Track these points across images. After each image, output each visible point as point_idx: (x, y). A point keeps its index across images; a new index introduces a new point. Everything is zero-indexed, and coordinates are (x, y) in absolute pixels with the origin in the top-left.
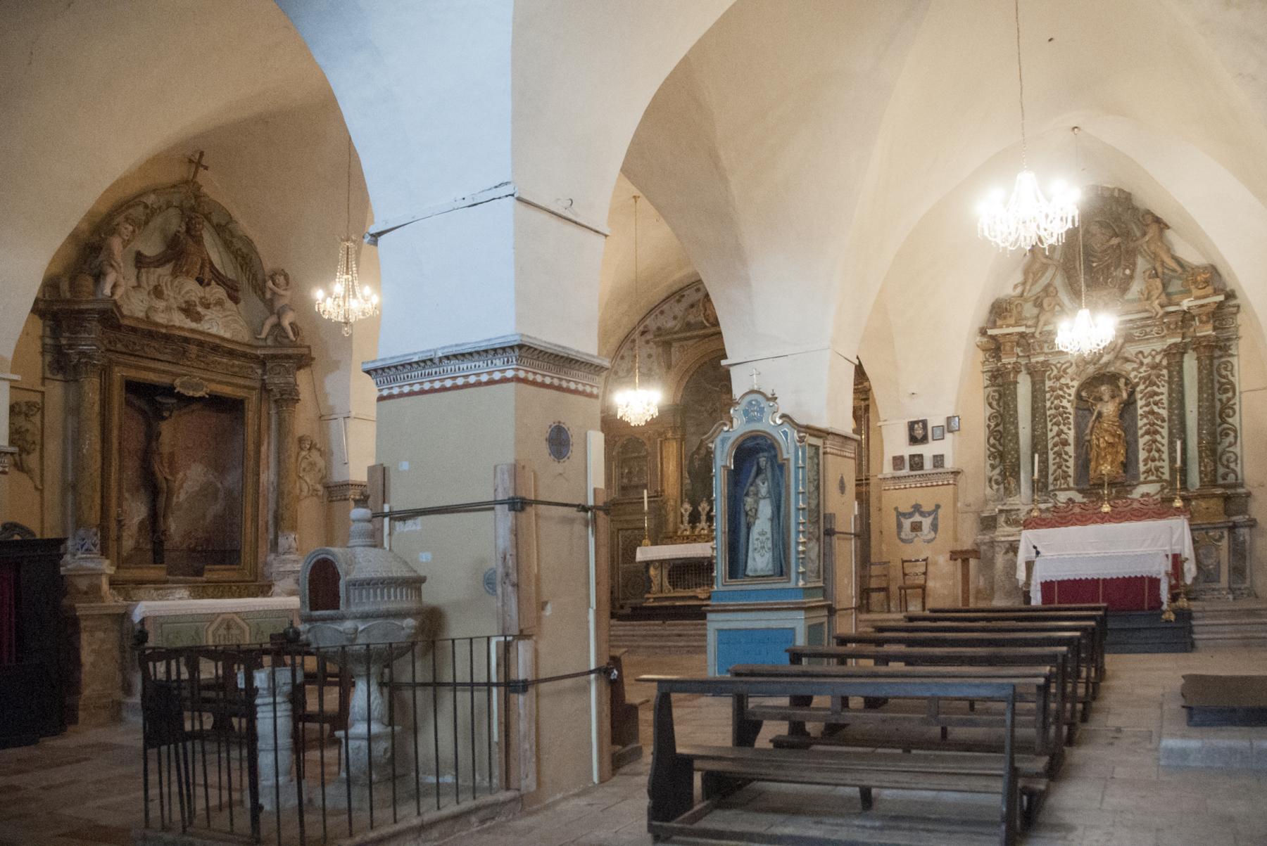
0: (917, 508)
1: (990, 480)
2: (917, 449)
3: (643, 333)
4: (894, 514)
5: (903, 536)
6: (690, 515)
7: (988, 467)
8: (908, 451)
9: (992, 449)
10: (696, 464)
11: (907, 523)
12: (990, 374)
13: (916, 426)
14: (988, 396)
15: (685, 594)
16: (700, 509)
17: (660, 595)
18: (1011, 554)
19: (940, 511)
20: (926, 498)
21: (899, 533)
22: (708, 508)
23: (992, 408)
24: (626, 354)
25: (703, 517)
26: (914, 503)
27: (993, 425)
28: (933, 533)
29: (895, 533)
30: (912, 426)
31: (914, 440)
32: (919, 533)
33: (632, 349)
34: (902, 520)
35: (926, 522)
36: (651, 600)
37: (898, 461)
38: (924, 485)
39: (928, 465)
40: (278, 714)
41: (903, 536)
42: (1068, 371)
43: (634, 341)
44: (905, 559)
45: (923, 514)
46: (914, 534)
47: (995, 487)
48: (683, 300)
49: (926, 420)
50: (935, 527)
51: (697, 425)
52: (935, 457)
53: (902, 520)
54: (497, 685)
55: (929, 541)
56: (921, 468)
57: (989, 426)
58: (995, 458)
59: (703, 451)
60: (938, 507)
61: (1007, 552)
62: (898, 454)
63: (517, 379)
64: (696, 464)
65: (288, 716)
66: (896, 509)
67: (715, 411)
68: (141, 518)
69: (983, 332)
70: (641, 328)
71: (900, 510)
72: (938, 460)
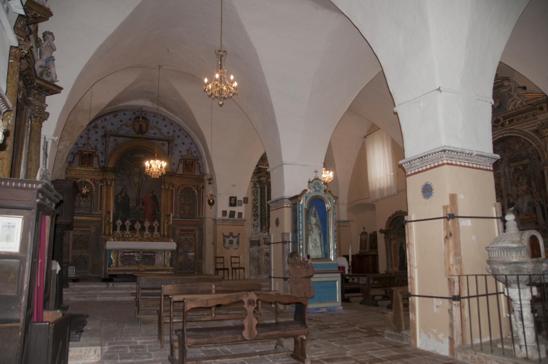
0: (231, 234)
1: (254, 225)
2: (233, 209)
3: (94, 127)
4: (222, 235)
5: (226, 246)
6: (121, 226)
7: (253, 220)
8: (229, 209)
9: (254, 213)
10: (119, 200)
11: (227, 240)
12: (254, 182)
13: (232, 199)
14: (253, 191)
15: (130, 269)
16: (126, 224)
17: (116, 269)
19: (240, 236)
20: (235, 230)
21: (224, 245)
22: (158, 225)
23: (255, 196)
25: (156, 229)
26: (230, 232)
27: (255, 203)
28: (237, 245)
29: (222, 244)
30: (231, 198)
31: (231, 205)
32: (232, 245)
33: (87, 134)
34: (226, 239)
35: (235, 240)
37: (224, 213)
38: (234, 224)
39: (236, 216)
40: (519, 302)
41: (226, 246)
42: (511, 202)
44: (232, 256)
45: (234, 237)
46: (230, 245)
47: (255, 228)
48: (117, 116)
49: (236, 197)
50: (238, 243)
52: (239, 213)
53: (226, 239)
54: (501, 293)
55: (236, 249)
56: (233, 217)
57: (253, 203)
58: (255, 216)
59: (123, 194)
60: (239, 234)
61: (265, 256)
62: (224, 209)
63: (448, 164)
64: (119, 200)
65: (528, 304)
66: (223, 233)
69: (257, 166)
71: (224, 234)
72: (240, 214)
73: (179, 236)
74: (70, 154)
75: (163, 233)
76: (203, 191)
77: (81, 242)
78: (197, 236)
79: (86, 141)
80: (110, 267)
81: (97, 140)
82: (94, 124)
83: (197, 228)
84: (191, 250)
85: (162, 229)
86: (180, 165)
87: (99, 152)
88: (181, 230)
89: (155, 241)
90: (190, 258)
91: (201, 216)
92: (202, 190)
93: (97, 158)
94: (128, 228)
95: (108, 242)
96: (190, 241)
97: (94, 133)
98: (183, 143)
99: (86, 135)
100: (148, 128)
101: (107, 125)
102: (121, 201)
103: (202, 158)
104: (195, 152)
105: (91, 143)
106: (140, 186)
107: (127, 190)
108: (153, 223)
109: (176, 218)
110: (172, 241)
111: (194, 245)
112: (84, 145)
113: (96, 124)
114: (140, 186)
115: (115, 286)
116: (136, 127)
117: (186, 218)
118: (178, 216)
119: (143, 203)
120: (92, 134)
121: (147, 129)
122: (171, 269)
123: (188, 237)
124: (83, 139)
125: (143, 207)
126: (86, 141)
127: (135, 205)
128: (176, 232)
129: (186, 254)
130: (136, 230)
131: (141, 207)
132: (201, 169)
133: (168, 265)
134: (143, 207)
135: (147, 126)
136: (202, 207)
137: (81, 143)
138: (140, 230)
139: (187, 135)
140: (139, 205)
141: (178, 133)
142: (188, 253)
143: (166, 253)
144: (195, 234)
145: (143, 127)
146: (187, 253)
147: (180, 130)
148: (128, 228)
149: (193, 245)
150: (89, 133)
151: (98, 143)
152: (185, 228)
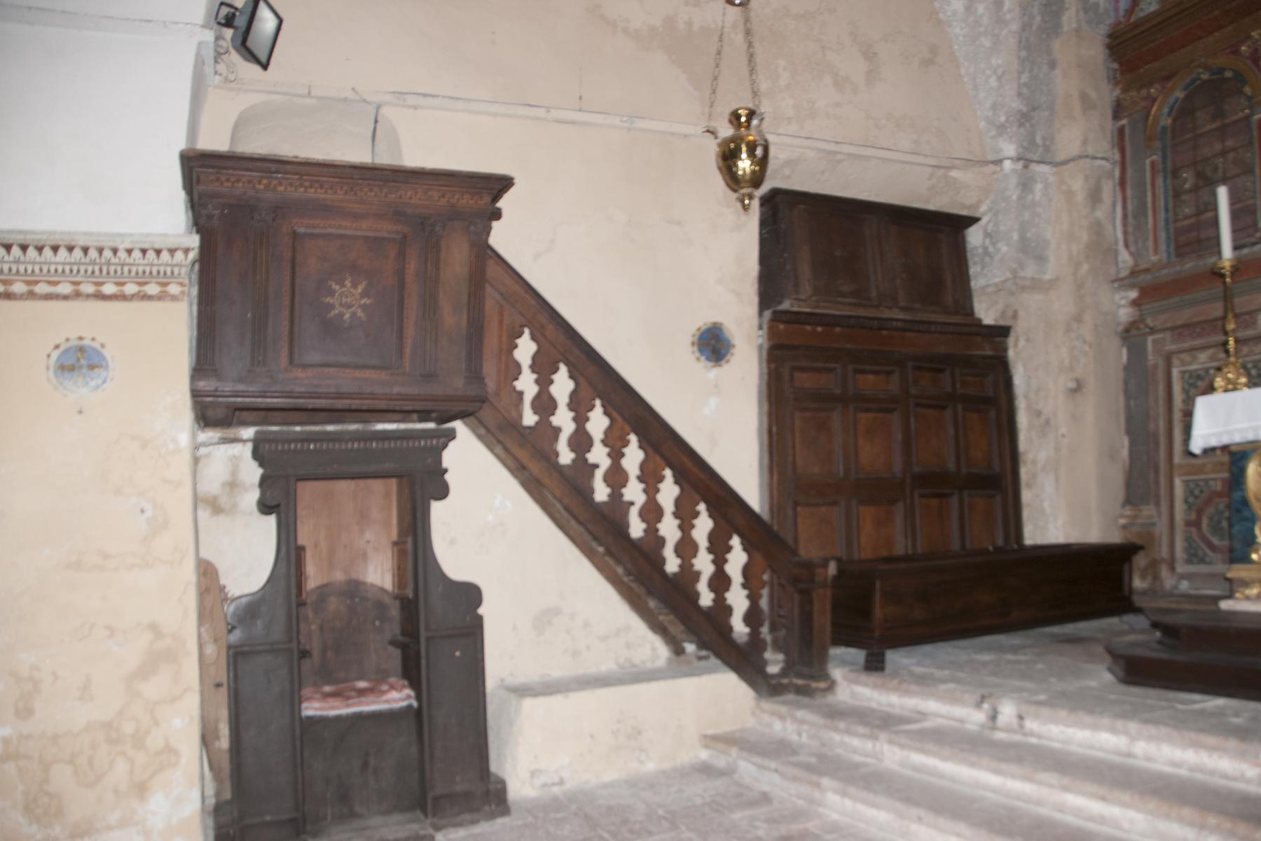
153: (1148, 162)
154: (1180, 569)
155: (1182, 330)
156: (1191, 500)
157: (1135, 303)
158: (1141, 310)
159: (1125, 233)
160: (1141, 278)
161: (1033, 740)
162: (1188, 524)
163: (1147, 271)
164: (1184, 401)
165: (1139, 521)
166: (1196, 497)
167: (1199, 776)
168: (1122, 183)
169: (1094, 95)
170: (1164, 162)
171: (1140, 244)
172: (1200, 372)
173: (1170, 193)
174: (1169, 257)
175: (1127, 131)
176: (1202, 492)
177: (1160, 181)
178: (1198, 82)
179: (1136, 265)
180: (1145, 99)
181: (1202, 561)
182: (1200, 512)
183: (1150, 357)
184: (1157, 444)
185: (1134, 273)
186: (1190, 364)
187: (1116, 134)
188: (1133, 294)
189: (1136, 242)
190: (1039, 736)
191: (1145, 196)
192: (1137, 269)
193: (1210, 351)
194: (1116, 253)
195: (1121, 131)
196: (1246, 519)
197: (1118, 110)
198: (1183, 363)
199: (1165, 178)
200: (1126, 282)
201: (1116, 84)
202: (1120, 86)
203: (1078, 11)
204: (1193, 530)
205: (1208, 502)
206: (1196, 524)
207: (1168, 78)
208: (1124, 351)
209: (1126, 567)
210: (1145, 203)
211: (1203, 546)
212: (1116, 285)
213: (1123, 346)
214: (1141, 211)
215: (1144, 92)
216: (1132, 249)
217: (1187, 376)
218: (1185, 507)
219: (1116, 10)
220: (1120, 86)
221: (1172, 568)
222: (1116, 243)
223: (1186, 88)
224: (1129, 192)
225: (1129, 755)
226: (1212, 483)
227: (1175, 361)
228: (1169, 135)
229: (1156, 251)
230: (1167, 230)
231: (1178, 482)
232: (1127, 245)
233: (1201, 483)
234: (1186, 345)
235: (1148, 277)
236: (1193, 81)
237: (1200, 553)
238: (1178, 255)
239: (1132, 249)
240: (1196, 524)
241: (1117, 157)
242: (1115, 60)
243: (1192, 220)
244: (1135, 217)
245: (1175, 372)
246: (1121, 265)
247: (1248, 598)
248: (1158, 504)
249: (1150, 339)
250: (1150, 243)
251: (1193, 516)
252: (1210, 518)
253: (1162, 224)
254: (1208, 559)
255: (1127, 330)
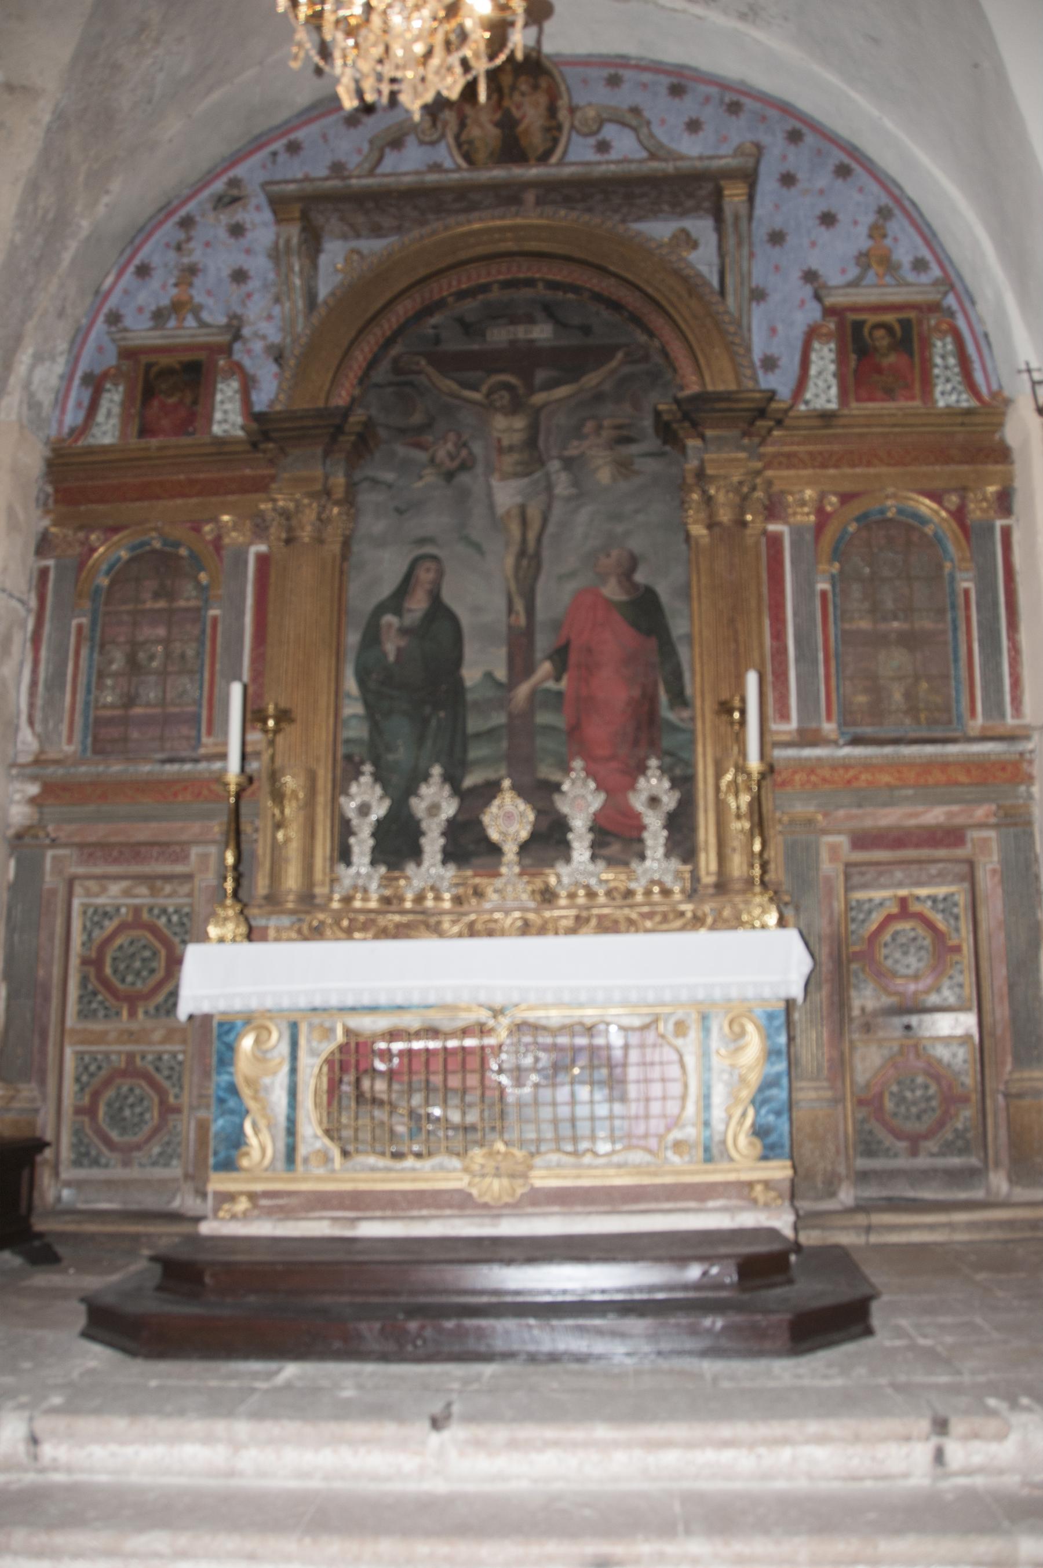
6: (380, 830)
10: (391, 647)
18: (615, 894)
22: (670, 801)
24: (156, 261)
25: (655, 837)
33: (179, 248)
36: (242, 1205)
43: (187, 223)
51: (399, 511)
59: (418, 604)
64: (391, 647)
67: (465, 466)
68: (662, 841)
70: (219, 186)
73: (848, 889)
74: (77, 381)
75: (713, 866)
76: (1007, 533)
77: (137, 964)
78: (988, 882)
79: (174, 291)
80: (228, 1165)
81: (240, 276)
82: (224, 179)
83: (981, 812)
84: (948, 995)
85: (706, 832)
86: (814, 356)
87: (258, 346)
88: (861, 841)
89: (647, 931)
90: (942, 1052)
91: (1010, 721)
92: (999, 523)
93: (235, 384)
94: (433, 844)
95: (194, 955)
96: (938, 919)
97: (222, 233)
98: (828, 219)
99: (172, 255)
100: (559, 128)
101: (685, 592)
102: (399, 651)
103: (973, 303)
104: (919, 265)
105: (199, 297)
106: (532, 536)
107: (440, 574)
108: (632, 786)
109: (814, 744)
110: (772, 918)
111: (967, 948)
112: (159, 316)
113: (234, 183)
114: (532, 536)
115: (48, 1451)
116: (475, 132)
117: (896, 741)
118: (829, 728)
119: (560, 657)
120: (207, 244)
121: (553, 131)
122: (767, 1184)
123: (923, 892)
124: (155, 283)
125: (563, 685)
126: (174, 291)
127: (501, 674)
128: (824, 855)
129: (908, 1027)
130: (495, 850)
131: (551, 685)
132: (979, 377)
133: (743, 1140)
134: (563, 685)
135: (552, 111)
136: (1015, 649)
137: (140, 310)
138: (524, 848)
139: (847, 160)
140: (529, 670)
141: (784, 157)
142: (927, 1018)
143: (718, 1026)
144: (971, 864)
145: (521, 127)
146: (914, 1020)
147: (794, 137)
148: (433, 844)
149: (957, 949)
150: (189, 239)
151: (249, 295)
152: (889, 817)
153: (75, 622)
154: (66, 1174)
155: (90, 851)
156: (85, 1078)
157: (33, 801)
158: (41, 813)
159: (31, 705)
160: (51, 770)
161: (59, 1477)
162: (78, 1111)
163: (56, 762)
164: (83, 944)
165: (16, 1105)
166: (92, 1075)
167: (338, 1485)
168: (36, 639)
169: (21, 516)
170: (93, 629)
171: (51, 725)
172: (108, 909)
173: (95, 671)
174: (84, 750)
175: (52, 576)
176: (99, 1068)
177: (84, 652)
178: (148, 548)
179: (42, 751)
180: (82, 544)
181: (95, 1162)
182: (96, 1095)
183: (48, 878)
184: (47, 998)
185: (37, 762)
186: (97, 895)
187: (35, 574)
188: (33, 789)
189: (45, 721)
190: (69, 1470)
191: (66, 665)
192: (43, 757)
193: (124, 884)
194: (17, 729)
195: (44, 573)
196: (232, 1112)
197: (44, 545)
198: (88, 893)
199: (92, 649)
200: (28, 771)
201: (47, 512)
202: (52, 516)
203: (21, 402)
204: (86, 1119)
205: (107, 1083)
206: (90, 1111)
207: (115, 529)
208: (12, 864)
209: (26, 1173)
210: (64, 675)
211: (96, 1140)
212: (14, 771)
213: (10, 856)
214: (56, 682)
215: (81, 535)
216: (38, 728)
217: (90, 911)
218: (77, 1088)
219: (61, 422)
220: (52, 516)
221: (56, 1174)
222: (18, 715)
223: (133, 548)
224: (43, 653)
225: (231, 1474)
226: (113, 1057)
227: (78, 889)
228: (103, 599)
229: (70, 740)
230: (86, 717)
231: (69, 1051)
232: (31, 722)
233: (99, 1057)
234: (98, 870)
235: (61, 771)
236: (142, 544)
237: (93, 1153)
238: (95, 752)
239: (38, 728)
240: (90, 1111)
241: (33, 603)
242: (51, 482)
243: (117, 712)
244: (48, 688)
245: (76, 903)
246: (20, 746)
247: (234, 1217)
248: (42, 1082)
249: (50, 853)
250: (64, 728)
251: (86, 1100)
252: (109, 1105)
253: (79, 706)
254: (103, 1161)
255: (19, 836)
